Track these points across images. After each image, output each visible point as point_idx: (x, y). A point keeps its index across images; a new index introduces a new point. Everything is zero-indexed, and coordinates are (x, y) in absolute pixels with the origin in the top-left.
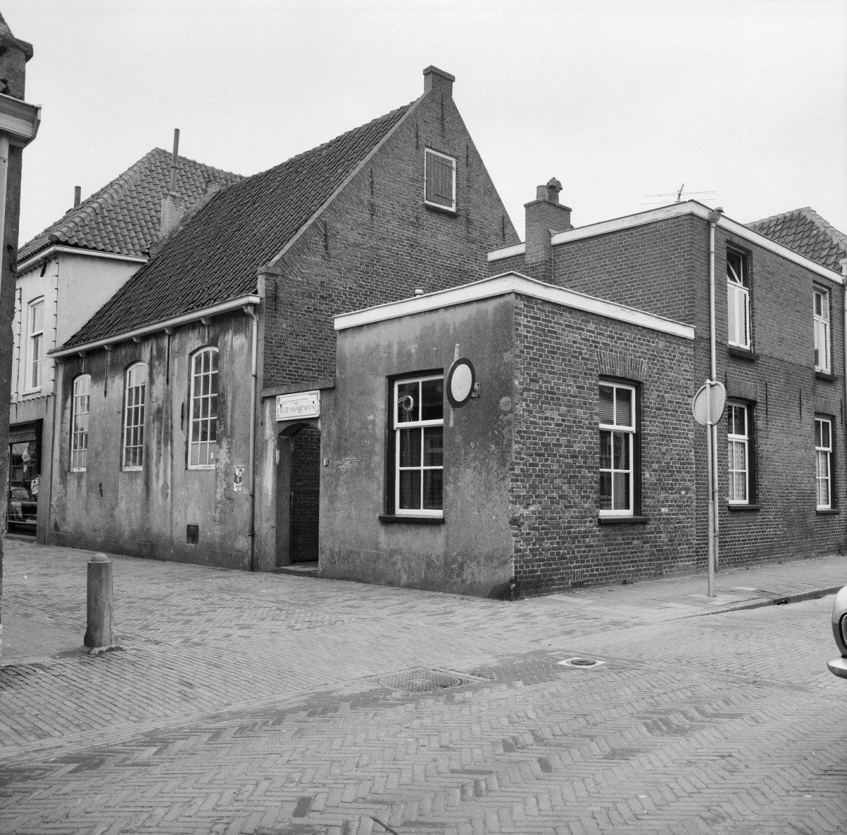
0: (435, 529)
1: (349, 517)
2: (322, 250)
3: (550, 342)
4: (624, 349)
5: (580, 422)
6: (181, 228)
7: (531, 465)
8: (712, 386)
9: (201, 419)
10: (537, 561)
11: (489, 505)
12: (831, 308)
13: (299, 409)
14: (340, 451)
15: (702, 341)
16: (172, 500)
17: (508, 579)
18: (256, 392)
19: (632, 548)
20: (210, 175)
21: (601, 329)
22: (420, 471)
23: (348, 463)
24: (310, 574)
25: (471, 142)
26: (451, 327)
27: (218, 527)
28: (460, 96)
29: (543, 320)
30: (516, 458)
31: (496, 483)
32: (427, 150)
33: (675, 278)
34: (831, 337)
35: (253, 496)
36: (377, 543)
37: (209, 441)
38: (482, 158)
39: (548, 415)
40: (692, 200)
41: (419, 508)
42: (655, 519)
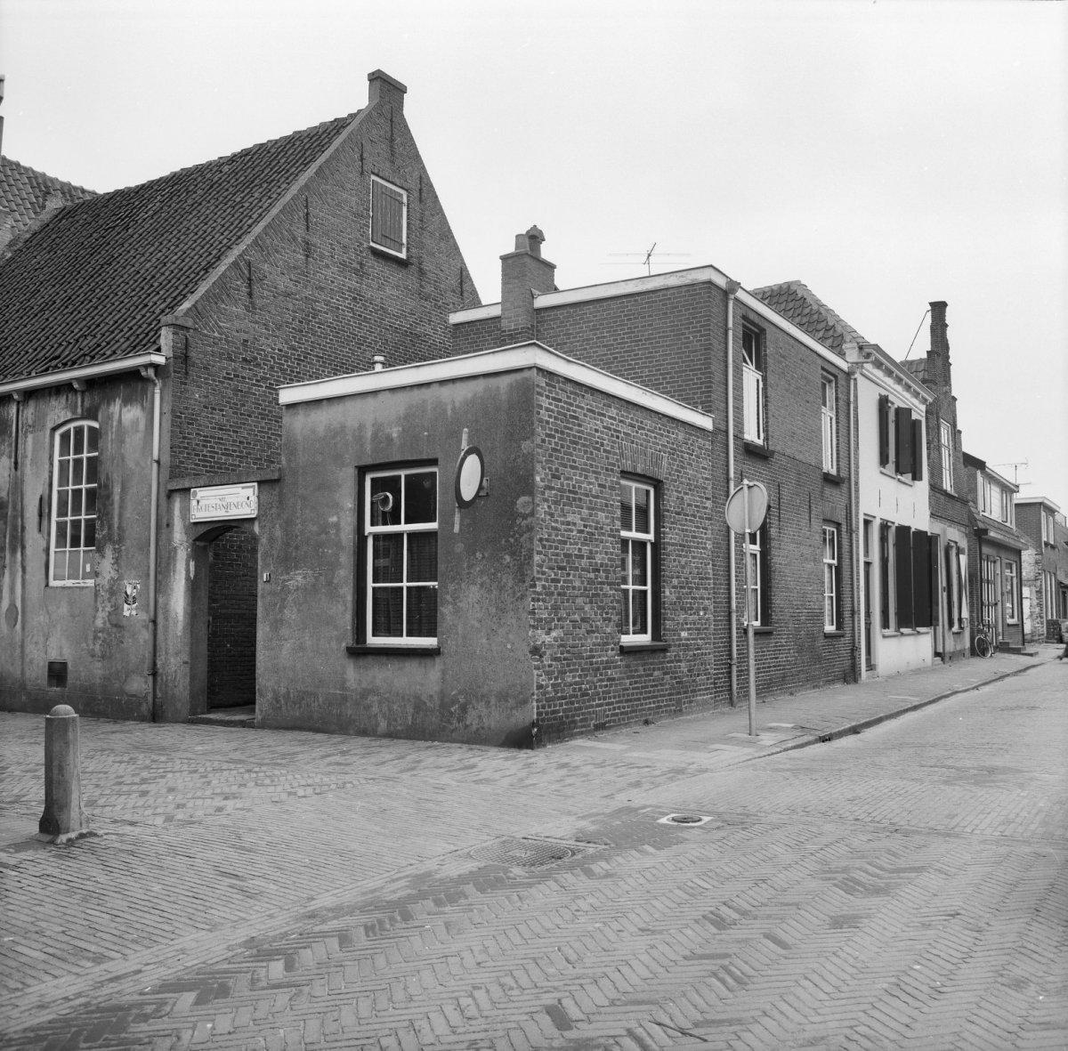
0: (428, 662)
1: (302, 648)
2: (245, 298)
3: (571, 429)
4: (645, 440)
5: (602, 528)
6: (10, 255)
7: (553, 581)
8: (749, 487)
9: (69, 518)
10: (559, 698)
11: (502, 631)
12: (837, 399)
13: (227, 507)
14: (288, 561)
15: (720, 432)
16: (23, 629)
17: (527, 722)
18: (159, 483)
19: (654, 681)
20: (43, 186)
21: (622, 416)
22: (401, 588)
23: (299, 578)
24: (243, 724)
25: (425, 172)
26: (449, 407)
27: (99, 665)
28: (413, 111)
29: (566, 402)
30: (538, 572)
31: (512, 603)
32: (373, 177)
33: (689, 356)
34: (837, 433)
35: (154, 622)
36: (344, 681)
37: (82, 548)
38: (438, 193)
39: (569, 519)
40: (711, 266)
41: (402, 636)
42: (675, 645)
